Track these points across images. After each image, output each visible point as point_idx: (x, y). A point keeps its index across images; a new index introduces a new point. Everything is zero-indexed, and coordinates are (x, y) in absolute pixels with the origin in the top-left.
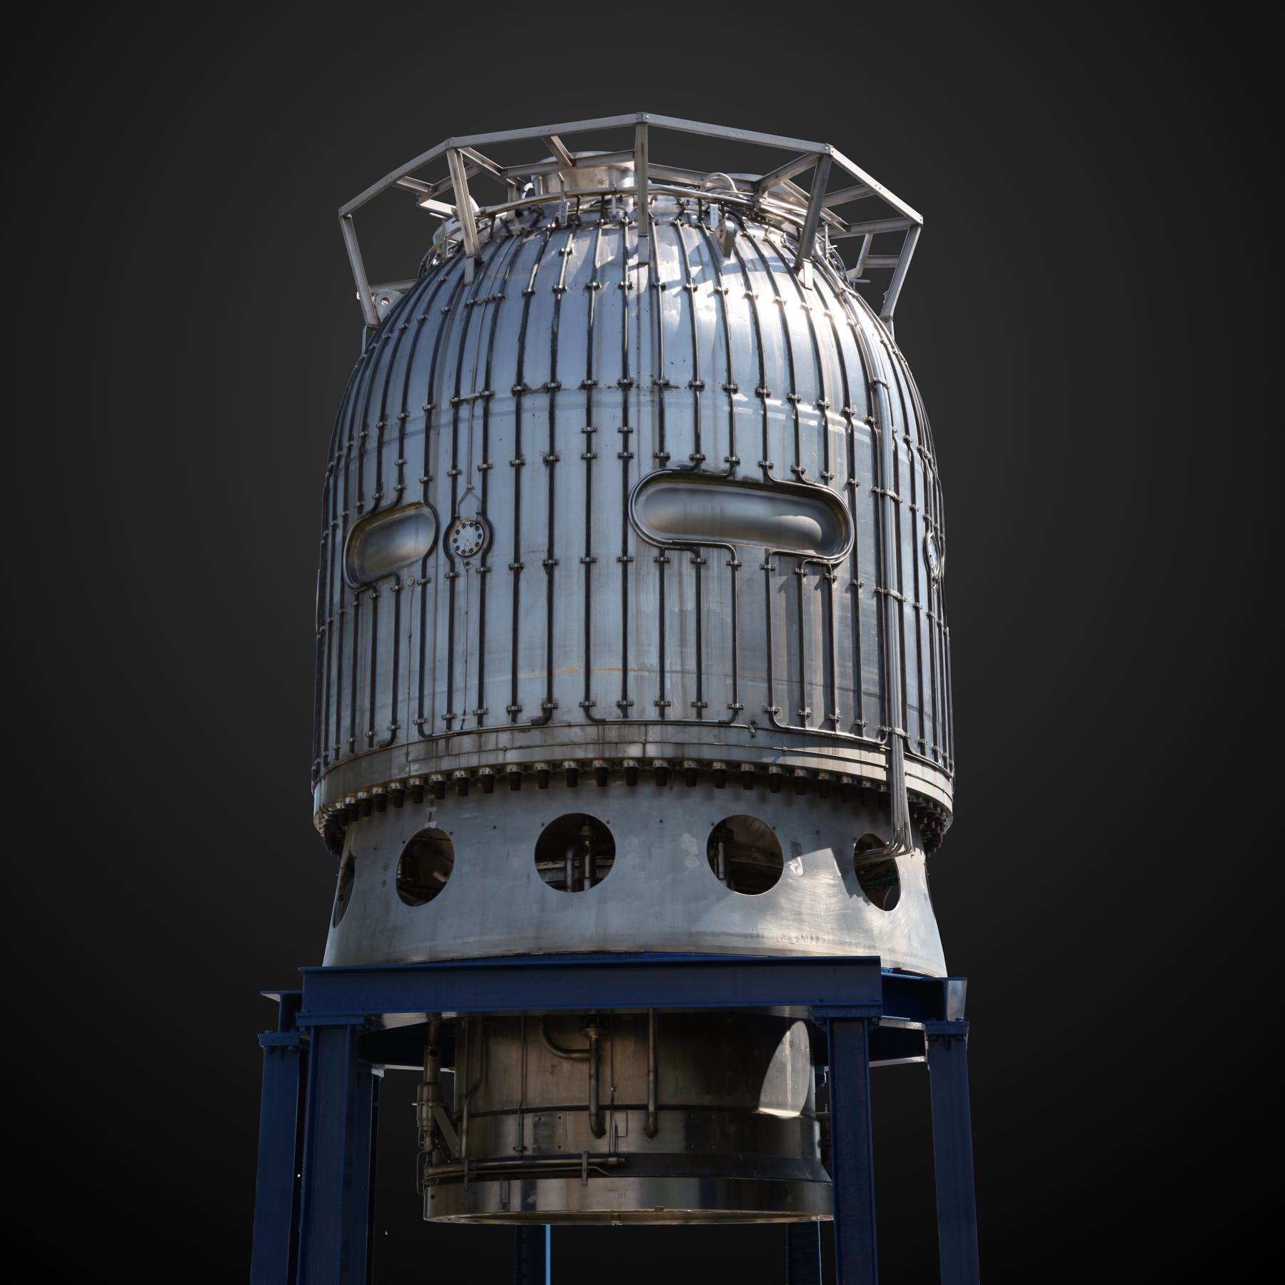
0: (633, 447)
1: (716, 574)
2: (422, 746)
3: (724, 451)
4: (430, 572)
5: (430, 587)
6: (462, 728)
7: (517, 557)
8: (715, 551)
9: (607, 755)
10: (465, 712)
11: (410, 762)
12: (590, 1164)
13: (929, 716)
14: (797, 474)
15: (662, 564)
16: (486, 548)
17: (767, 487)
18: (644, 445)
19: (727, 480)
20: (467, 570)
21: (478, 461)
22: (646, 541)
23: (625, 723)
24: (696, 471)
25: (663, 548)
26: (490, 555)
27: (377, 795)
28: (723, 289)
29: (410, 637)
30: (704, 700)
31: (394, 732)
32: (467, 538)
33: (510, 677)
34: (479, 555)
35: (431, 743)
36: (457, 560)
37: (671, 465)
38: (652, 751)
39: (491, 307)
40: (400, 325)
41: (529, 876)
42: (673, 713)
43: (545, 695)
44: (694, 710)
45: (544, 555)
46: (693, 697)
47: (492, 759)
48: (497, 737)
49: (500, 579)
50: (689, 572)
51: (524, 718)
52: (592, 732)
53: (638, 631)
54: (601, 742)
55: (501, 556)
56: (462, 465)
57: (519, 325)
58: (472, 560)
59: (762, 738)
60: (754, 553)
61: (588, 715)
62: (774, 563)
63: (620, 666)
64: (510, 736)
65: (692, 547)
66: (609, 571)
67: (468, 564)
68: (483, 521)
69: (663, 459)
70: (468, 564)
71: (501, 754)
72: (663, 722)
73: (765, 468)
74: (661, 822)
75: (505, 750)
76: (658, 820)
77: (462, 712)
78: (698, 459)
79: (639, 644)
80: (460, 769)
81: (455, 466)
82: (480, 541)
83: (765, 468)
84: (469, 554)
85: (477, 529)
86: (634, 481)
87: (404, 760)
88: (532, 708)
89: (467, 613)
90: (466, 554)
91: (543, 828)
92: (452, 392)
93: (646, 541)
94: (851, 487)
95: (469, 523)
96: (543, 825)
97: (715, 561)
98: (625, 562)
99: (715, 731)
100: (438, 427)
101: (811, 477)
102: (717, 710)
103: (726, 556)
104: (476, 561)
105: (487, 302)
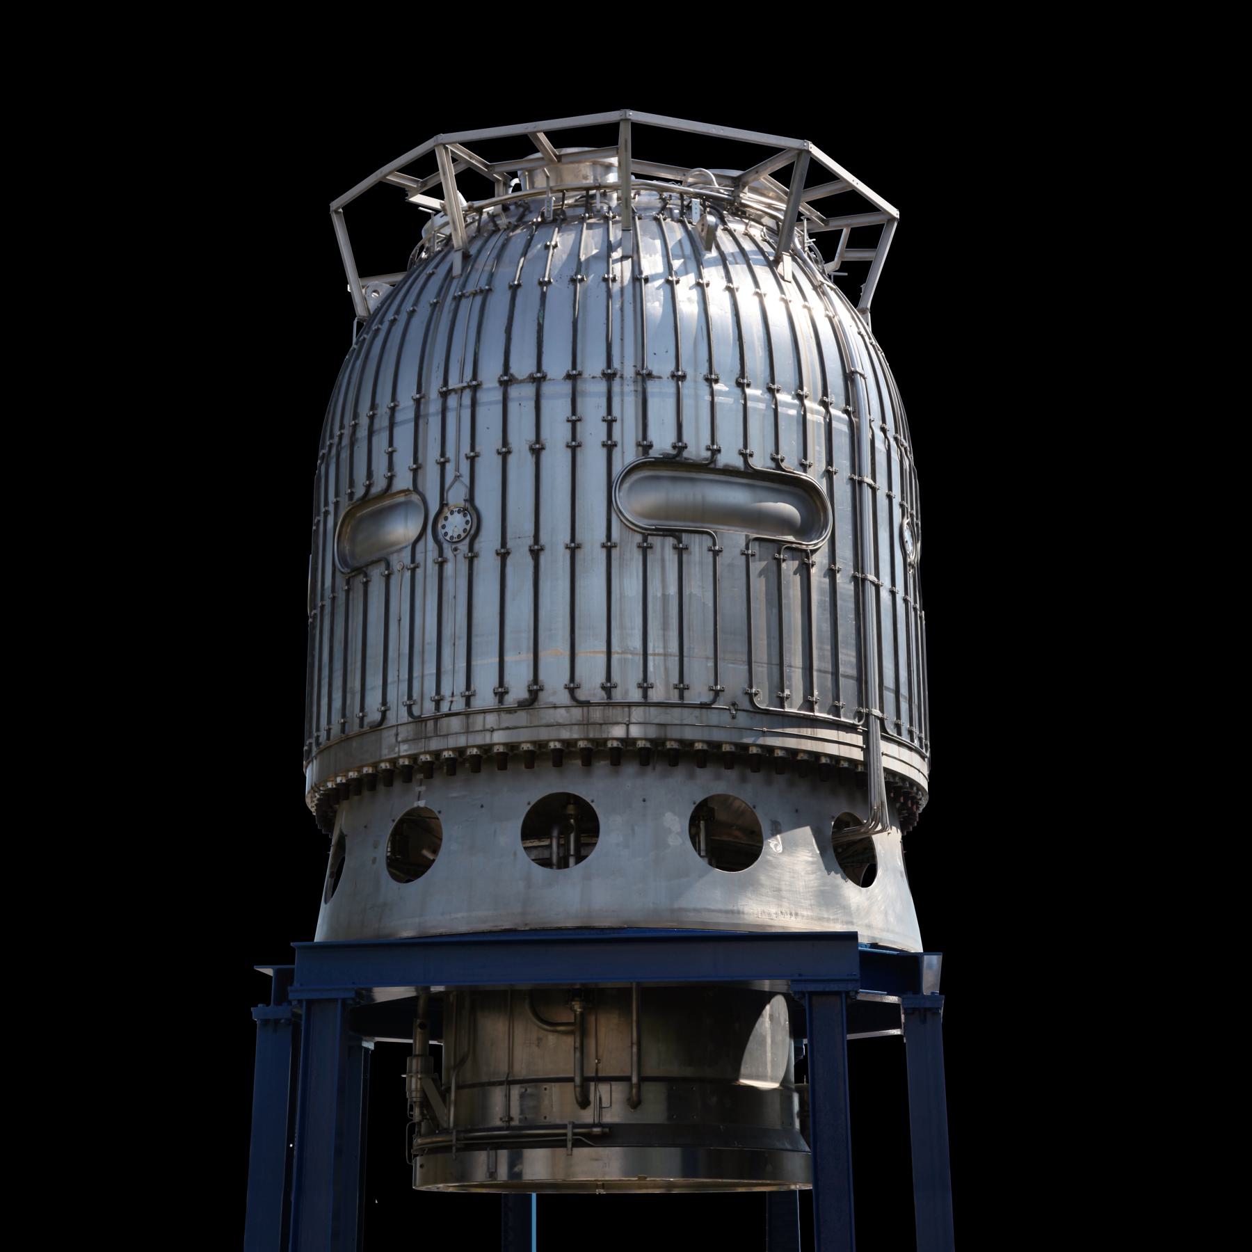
0: (616, 436)
1: (697, 559)
2: (411, 727)
3: (706, 440)
4: (419, 557)
5: (419, 572)
6: (450, 710)
7: (504, 543)
8: (697, 537)
9: (591, 736)
10: (453, 693)
11: (399, 742)
12: (574, 1134)
14: (777, 462)
15: (645, 550)
16: (473, 534)
17: (747, 475)
18: (627, 434)
19: (708, 468)
20: (455, 556)
21: (466, 449)
22: (629, 527)
23: (609, 704)
24: (678, 459)
25: (646, 534)
26: (477, 541)
27: (368, 775)
28: (704, 281)
29: (400, 620)
30: (686, 682)
31: (384, 714)
32: (455, 524)
33: (497, 660)
34: (467, 541)
35: (420, 724)
36: (446, 545)
37: (654, 453)
38: (635, 731)
39: (479, 299)
40: (390, 316)
41: (515, 854)
42: (656, 695)
43: (531, 677)
44: (676, 692)
45: (530, 541)
46: (675, 679)
47: (479, 740)
48: (484, 718)
49: (487, 564)
50: (671, 558)
52: (577, 713)
53: (621, 615)
54: (586, 723)
55: (488, 542)
56: (450, 453)
57: (506, 317)
58: (460, 546)
60: (735, 538)
61: (573, 697)
62: (754, 548)
63: (604, 649)
66: (593, 557)
67: (456, 549)
68: (470, 508)
69: (646, 447)
70: (456, 549)
71: (488, 735)
72: (646, 703)
73: (745, 456)
74: (644, 801)
75: (492, 730)
76: (641, 799)
77: (450, 694)
78: (680, 447)
79: (622, 627)
80: (448, 749)
81: (443, 454)
82: (468, 527)
83: (745, 456)
84: (457, 540)
85: (465, 515)
86: (618, 469)
87: (393, 740)
88: (518, 690)
89: (455, 597)
90: (454, 540)
91: (529, 807)
92: (441, 382)
93: (629, 527)
94: (829, 475)
95: (457, 509)
96: (529, 804)
97: (697, 546)
98: (609, 547)
99: (697, 712)
100: (427, 416)
101: (790, 465)
102: (699, 692)
103: (708, 542)
104: (464, 547)
105: (475, 294)
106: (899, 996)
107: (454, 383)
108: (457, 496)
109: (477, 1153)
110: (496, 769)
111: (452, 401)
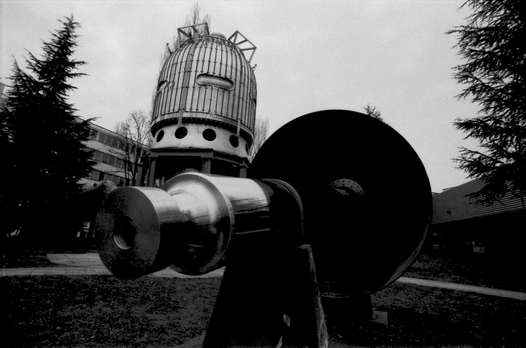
8: (209, 87)
13: (466, 155)
15: (200, 88)
16: (173, 86)
18: (199, 70)
21: (174, 72)
22: (198, 84)
23: (197, 112)
25: (200, 85)
32: (171, 85)
37: (204, 73)
39: (175, 65)
40: (165, 68)
42: (223, 115)
51: (175, 111)
55: (175, 87)
59: (215, 116)
61: (216, 114)
64: (265, 205)
65: (204, 85)
68: (174, 81)
69: (202, 72)
72: (221, 116)
78: (208, 72)
86: (197, 75)
88: (206, 111)
93: (198, 84)
98: (194, 87)
103: (211, 87)
105: (175, 64)
106: (269, 206)
107: (174, 63)
108: (172, 80)
109: (156, 211)
110: (321, 347)
111: (174, 66)
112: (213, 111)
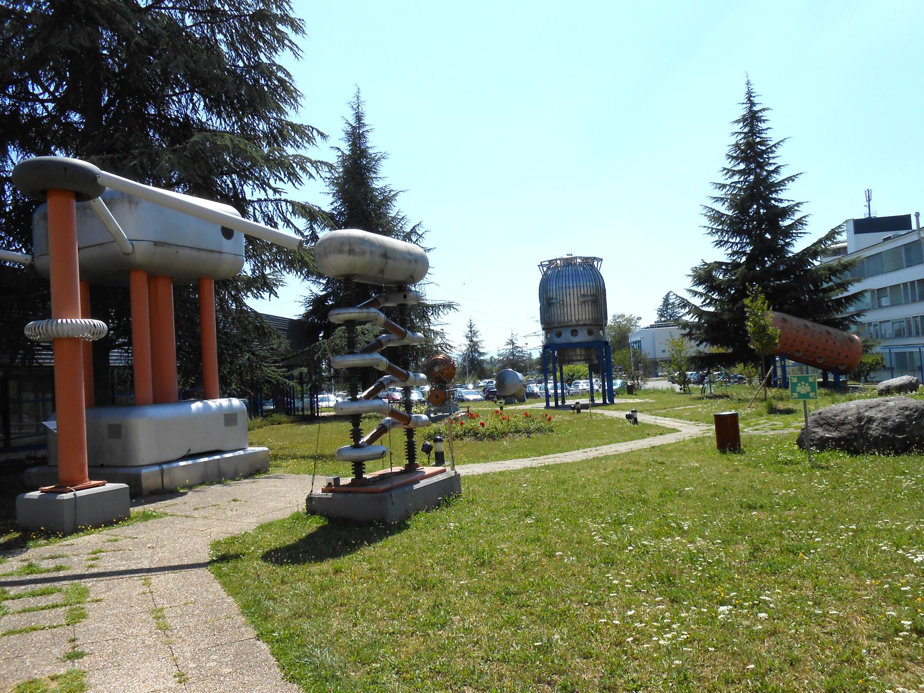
49: (565, 306)
68: (563, 300)
88: (570, 320)
108: (561, 299)
112: (556, 322)
